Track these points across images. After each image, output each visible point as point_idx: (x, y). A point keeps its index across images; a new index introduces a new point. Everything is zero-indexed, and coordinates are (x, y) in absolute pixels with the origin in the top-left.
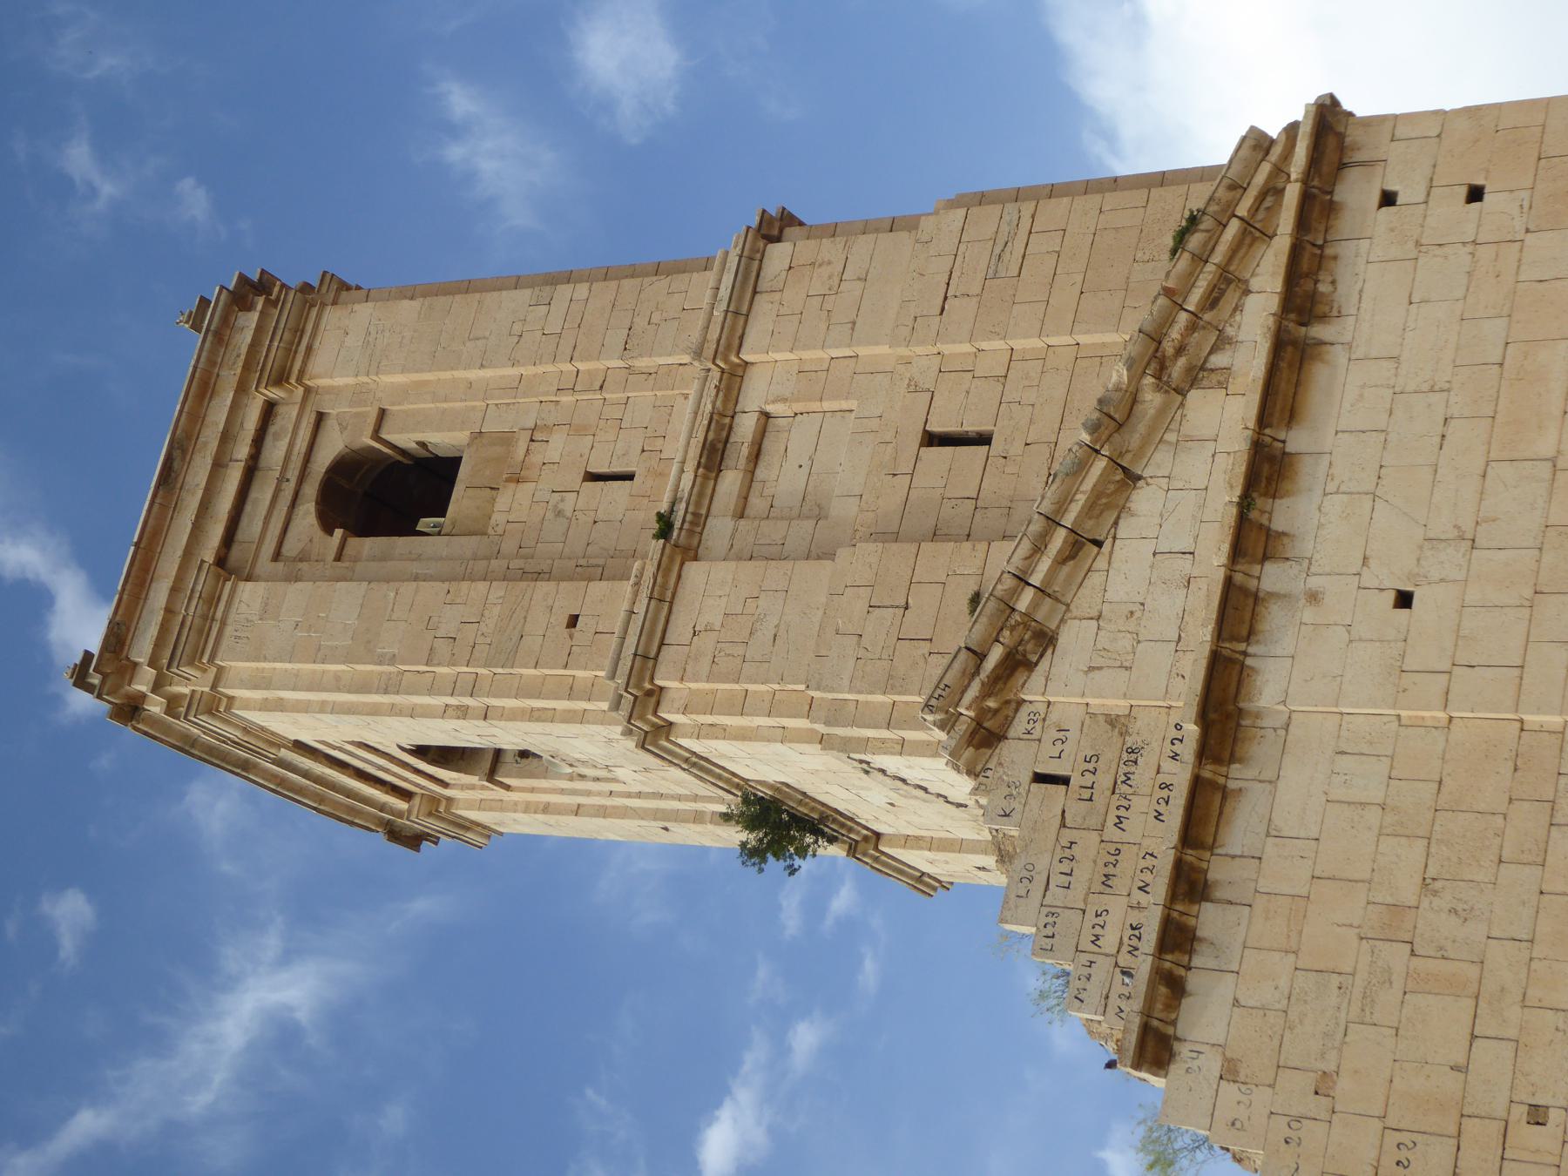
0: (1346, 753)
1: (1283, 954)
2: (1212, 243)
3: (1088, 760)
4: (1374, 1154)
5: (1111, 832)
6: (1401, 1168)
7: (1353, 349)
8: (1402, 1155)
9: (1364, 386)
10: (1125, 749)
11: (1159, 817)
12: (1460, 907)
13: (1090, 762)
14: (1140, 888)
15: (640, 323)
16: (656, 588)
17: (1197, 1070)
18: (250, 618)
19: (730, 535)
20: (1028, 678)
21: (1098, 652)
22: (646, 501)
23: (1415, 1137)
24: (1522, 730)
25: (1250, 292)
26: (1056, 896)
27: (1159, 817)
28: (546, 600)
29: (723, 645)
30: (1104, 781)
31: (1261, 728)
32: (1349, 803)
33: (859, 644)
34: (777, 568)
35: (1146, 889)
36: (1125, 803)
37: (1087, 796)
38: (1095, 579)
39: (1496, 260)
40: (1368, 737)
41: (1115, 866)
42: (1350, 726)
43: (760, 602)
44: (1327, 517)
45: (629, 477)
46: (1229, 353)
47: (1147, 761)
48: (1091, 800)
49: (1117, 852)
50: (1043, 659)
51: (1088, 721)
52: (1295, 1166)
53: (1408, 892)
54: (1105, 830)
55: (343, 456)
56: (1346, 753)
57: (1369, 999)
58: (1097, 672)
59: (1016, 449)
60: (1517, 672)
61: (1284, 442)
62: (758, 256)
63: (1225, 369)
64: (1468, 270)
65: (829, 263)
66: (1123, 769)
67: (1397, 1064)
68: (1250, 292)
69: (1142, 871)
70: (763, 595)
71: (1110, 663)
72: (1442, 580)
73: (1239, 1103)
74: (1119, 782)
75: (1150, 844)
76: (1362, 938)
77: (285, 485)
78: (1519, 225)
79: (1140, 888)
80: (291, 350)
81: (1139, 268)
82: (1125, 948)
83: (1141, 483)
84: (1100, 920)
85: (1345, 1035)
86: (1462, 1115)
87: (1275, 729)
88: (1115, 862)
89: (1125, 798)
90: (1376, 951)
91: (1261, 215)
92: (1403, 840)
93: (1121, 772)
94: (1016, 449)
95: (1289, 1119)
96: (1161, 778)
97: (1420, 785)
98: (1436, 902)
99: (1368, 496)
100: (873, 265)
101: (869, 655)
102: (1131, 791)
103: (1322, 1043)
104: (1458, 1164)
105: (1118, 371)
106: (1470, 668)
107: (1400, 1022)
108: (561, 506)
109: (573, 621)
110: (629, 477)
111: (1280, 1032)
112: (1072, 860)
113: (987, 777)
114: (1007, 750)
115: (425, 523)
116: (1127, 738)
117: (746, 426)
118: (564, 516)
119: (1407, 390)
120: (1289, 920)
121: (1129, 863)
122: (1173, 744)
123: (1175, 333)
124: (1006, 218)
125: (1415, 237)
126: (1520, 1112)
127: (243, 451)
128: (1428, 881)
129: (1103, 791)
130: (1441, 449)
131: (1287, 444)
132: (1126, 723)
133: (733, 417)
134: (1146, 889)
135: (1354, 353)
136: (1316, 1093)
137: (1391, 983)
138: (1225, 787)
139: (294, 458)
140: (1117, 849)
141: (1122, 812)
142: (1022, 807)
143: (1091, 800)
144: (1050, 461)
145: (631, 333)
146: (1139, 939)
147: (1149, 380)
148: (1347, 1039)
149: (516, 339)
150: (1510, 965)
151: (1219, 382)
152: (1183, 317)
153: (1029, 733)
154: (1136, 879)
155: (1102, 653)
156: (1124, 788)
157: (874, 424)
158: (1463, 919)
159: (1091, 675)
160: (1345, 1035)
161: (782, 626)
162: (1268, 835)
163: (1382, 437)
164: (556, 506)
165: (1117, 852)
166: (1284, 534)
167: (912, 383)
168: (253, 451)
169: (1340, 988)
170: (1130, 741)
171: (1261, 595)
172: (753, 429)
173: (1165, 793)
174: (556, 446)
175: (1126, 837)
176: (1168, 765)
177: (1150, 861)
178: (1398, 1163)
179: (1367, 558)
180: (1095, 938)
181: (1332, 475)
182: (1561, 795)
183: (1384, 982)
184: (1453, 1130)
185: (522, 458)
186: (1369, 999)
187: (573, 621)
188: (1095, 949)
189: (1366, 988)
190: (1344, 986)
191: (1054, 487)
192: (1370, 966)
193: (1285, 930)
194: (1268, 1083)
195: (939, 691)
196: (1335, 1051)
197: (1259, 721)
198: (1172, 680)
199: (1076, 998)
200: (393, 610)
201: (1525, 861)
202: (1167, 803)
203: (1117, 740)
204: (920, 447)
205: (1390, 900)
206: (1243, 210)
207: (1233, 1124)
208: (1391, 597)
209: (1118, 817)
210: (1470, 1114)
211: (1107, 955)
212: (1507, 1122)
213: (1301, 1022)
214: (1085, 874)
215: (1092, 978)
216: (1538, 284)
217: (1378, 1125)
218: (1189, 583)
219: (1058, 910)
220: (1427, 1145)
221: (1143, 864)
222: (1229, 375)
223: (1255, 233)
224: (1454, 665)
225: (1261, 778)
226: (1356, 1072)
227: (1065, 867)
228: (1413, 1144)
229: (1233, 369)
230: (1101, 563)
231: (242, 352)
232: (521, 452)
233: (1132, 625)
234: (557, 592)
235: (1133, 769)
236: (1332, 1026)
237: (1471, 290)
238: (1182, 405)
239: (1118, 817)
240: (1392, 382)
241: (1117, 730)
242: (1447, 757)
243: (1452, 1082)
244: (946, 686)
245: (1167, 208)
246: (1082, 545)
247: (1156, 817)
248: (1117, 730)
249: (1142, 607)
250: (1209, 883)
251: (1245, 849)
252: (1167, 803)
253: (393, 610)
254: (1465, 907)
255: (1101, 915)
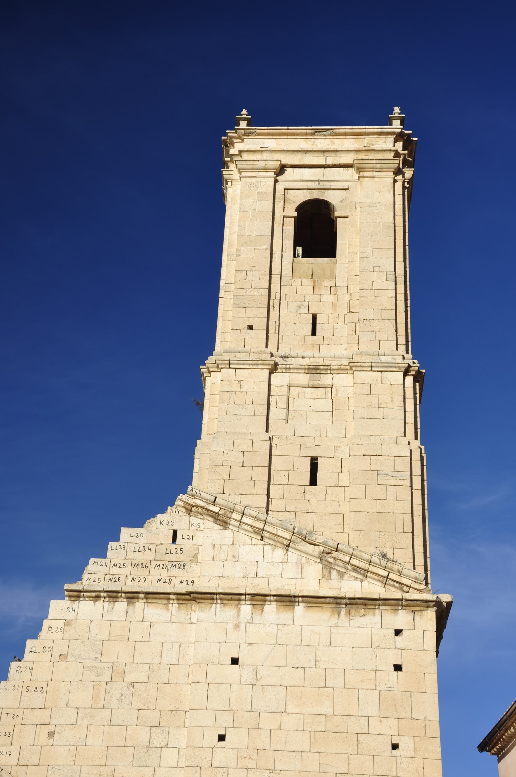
0: (180, 647)
1: (108, 635)
2: (377, 566)
3: (181, 550)
4: (39, 679)
5: (154, 563)
6: (35, 689)
7: (335, 627)
8: (39, 689)
9: (320, 634)
10: (185, 563)
11: (159, 581)
12: (123, 697)
13: (180, 550)
14: (133, 578)
15: (375, 323)
16: (256, 362)
17: (69, 611)
18: (258, 188)
19: (281, 384)
20: (211, 521)
21: (220, 547)
22: (303, 343)
23: (45, 693)
24: (186, 711)
25: (362, 582)
26: (131, 547)
27: (159, 581)
28: (259, 314)
29: (234, 394)
30: (173, 557)
31: (191, 613)
32: (162, 651)
33: (229, 451)
34: (264, 409)
35: (133, 580)
36: (164, 567)
37: (167, 552)
38: (248, 540)
39: (368, 680)
40: (185, 654)
41: (142, 567)
42: (190, 647)
43: (251, 405)
44: (268, 627)
45: (314, 333)
46: (337, 578)
47: (180, 573)
48: (166, 553)
49: (146, 567)
50: (218, 526)
51: (196, 547)
52: (36, 652)
53: (129, 678)
54: (155, 561)
55: (330, 204)
56: (180, 647)
57: (92, 669)
58: (212, 547)
59: (307, 496)
60: (205, 708)
61: (299, 605)
62: (397, 369)
63: (330, 577)
64: (365, 669)
65: (392, 401)
66: (177, 564)
67: (70, 682)
68: (362, 582)
69: (139, 578)
70: (253, 406)
71: (216, 552)
72: (241, 676)
73: (57, 628)
74: (172, 563)
75: (149, 579)
76: (113, 663)
77: (317, 183)
78: (383, 687)
79: (133, 578)
80: (373, 169)
81: (377, 534)
82: (111, 577)
83: (285, 551)
84: (122, 565)
85: (80, 662)
86: (51, 708)
87: (190, 619)
88: (143, 567)
89: (166, 566)
90: (109, 669)
91: (391, 582)
92: (147, 673)
93: (176, 563)
94: (307, 496)
95: (52, 647)
96: (173, 578)
97: (168, 677)
98: (125, 688)
99: (276, 642)
100: (390, 420)
101: (225, 456)
102: (169, 568)
103: (77, 654)
104: (35, 709)
105: (322, 538)
106: (207, 690)
107: (84, 681)
108: (303, 307)
109: (251, 327)
110: (314, 333)
111: (81, 639)
112: (144, 551)
113: (175, 513)
114: (186, 517)
115: (300, 249)
116: (189, 563)
117: (327, 379)
118: (298, 310)
119: (317, 651)
120: (120, 635)
121: (142, 572)
122: (186, 581)
123: (341, 556)
124: (404, 474)
125: (381, 646)
126: (52, 728)
127: (330, 160)
128: (133, 684)
129: (169, 558)
130: (292, 667)
131: (298, 607)
132: (195, 562)
133: (331, 373)
134: (133, 580)
135: (334, 628)
136: (60, 655)
137: (97, 676)
138: (170, 603)
139: (329, 184)
140: (147, 567)
141: (161, 566)
142: (164, 528)
143: (166, 553)
144: (302, 511)
145: (371, 320)
146: (115, 581)
147: (322, 549)
148: (78, 663)
149: (372, 270)
150: (102, 718)
151: (325, 575)
152: (347, 559)
153: (192, 525)
154: (136, 576)
155: (219, 548)
156: (170, 565)
157: (324, 434)
158: (118, 699)
159: (211, 546)
160: (80, 662)
161: (240, 417)
162: (151, 622)
163: (299, 644)
164: (303, 305)
165: (146, 567)
166: (262, 611)
167: (338, 448)
168: (331, 165)
169: (96, 658)
170: (187, 564)
171: (239, 606)
172: (325, 383)
173: (168, 581)
174: (328, 298)
175: (152, 569)
176: (178, 581)
177: (143, 580)
178: (36, 688)
179: (251, 645)
180: (115, 565)
181: (285, 626)
182: (161, 729)
183: (97, 674)
184: (47, 706)
185: (324, 284)
186: (92, 669)
187: (251, 327)
188: (111, 566)
189: (96, 667)
190: (97, 659)
191: (277, 521)
192: (103, 668)
193: (117, 635)
194: (64, 637)
195: (198, 491)
196: (74, 660)
197: (194, 612)
198: (208, 577)
199: (94, 562)
200: (259, 249)
201: (138, 719)
202: (164, 583)
203: (188, 559)
204: (311, 457)
205: (126, 671)
206: (391, 576)
207: (50, 627)
208: (236, 656)
209: (159, 565)
210: (52, 711)
211: (109, 571)
212: (49, 724)
213: (85, 646)
214: (139, 557)
215: (101, 567)
216: (357, 697)
217: (49, 679)
218: (245, 577)
219: (126, 549)
220: (42, 698)
221: (142, 578)
222: (327, 579)
223: (385, 580)
224: (209, 684)
225: (172, 616)
226: (67, 668)
227: (142, 549)
228: (42, 692)
229: (330, 580)
230: (255, 541)
231: (375, 146)
232: (326, 284)
233: (230, 558)
234: (262, 318)
235: (177, 567)
236: (83, 657)
237: (357, 671)
238: (316, 562)
239: (159, 565)
240: (321, 645)
241: (192, 558)
242: (177, 685)
243: (63, 704)
244: (200, 494)
245: (402, 541)
246: (260, 533)
247: (159, 579)
248: (192, 558)
249: (236, 561)
250: (134, 604)
251: (146, 615)
252: (164, 583)
253: (259, 249)
254: (123, 699)
255: (124, 565)
